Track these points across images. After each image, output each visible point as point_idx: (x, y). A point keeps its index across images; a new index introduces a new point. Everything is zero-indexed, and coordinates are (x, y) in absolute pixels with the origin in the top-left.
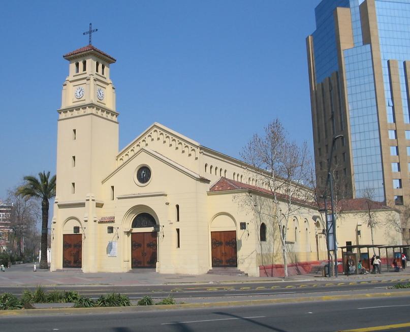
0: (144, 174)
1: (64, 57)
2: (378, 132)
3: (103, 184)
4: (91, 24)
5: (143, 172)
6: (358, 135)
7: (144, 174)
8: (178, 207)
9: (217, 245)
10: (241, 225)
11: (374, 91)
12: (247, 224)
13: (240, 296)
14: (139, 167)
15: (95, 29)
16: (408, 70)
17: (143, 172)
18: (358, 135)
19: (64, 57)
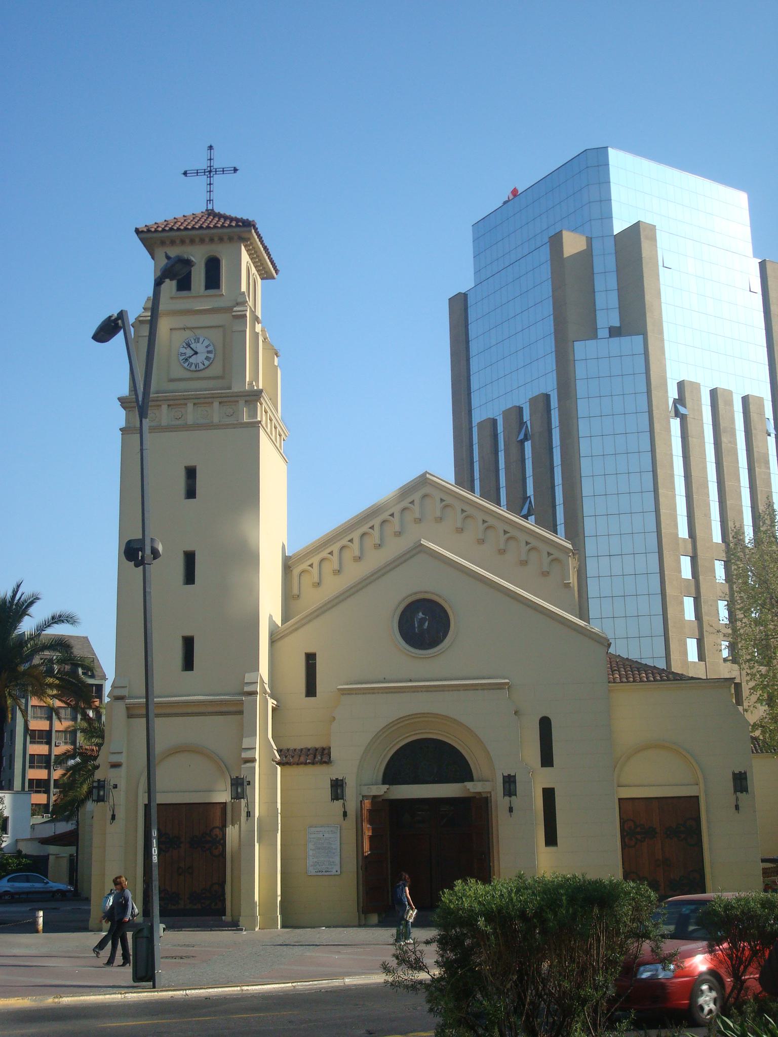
0: (422, 622)
1: (137, 231)
2: (656, 556)
3: (270, 615)
4: (211, 148)
5: (421, 615)
6: (604, 561)
7: (422, 622)
8: (545, 725)
9: (639, 837)
10: (332, 786)
11: (644, 376)
12: (245, 784)
13: (263, 982)
14: (410, 600)
15: (205, 154)
16: (773, 308)
17: (421, 615)
18: (604, 561)
19: (137, 231)
